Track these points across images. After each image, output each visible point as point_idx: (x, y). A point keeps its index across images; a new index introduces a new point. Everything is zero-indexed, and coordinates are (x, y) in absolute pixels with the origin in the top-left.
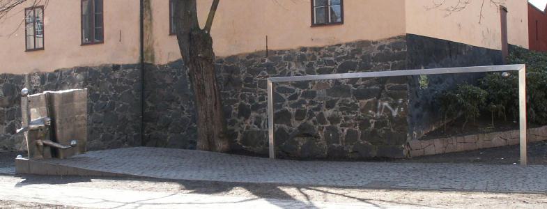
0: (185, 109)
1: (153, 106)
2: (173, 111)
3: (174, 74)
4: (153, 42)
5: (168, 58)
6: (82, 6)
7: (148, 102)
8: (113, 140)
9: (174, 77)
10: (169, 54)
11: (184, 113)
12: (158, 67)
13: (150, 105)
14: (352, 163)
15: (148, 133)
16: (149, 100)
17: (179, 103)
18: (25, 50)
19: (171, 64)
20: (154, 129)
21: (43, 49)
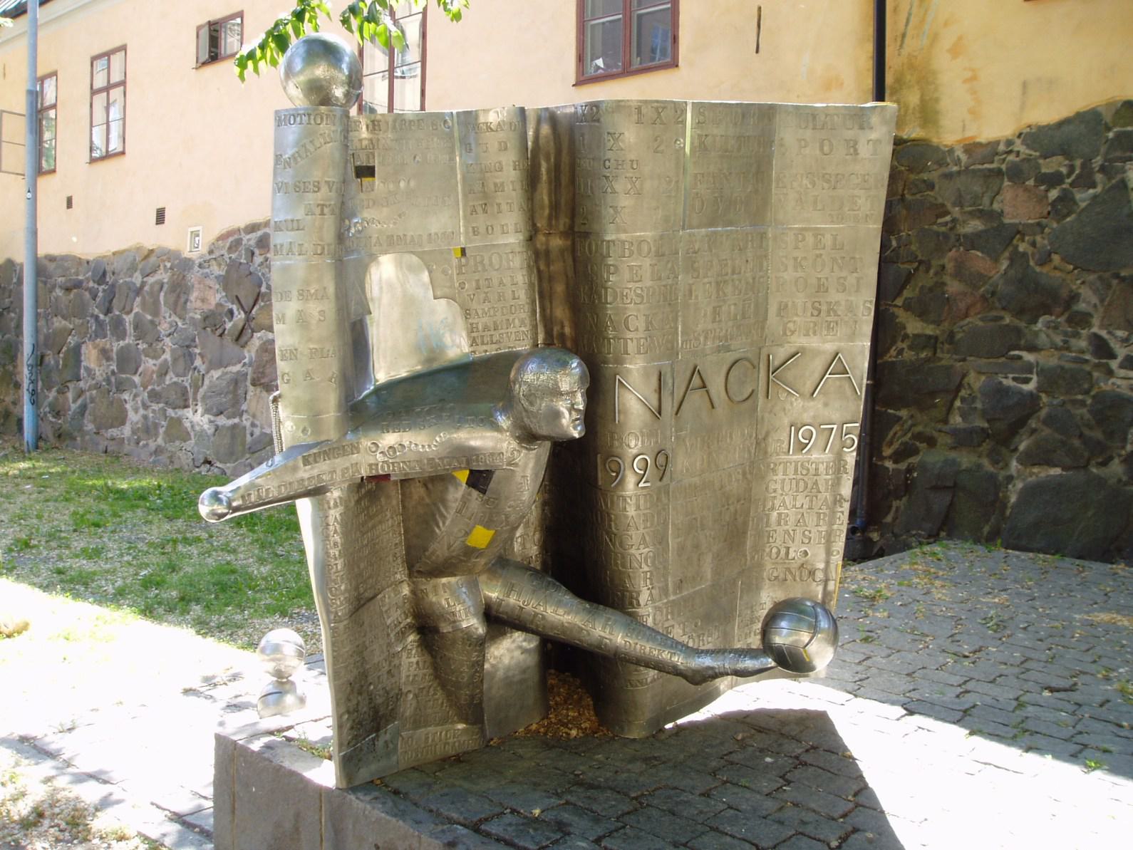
0: (1121, 352)
1: (930, 330)
2: (1049, 359)
3: (1053, 180)
4: (935, 38)
5: (1023, 107)
6: (198, 37)
7: (902, 316)
8: (248, 383)
9: (1054, 194)
10: (1025, 85)
11: (1110, 373)
12: (959, 153)
13: (914, 326)
14: (491, 479)
15: (897, 457)
16: (907, 307)
17: (1081, 320)
18: (572, 79)
19: (1036, 137)
20: (931, 442)
21: (123, 153)
